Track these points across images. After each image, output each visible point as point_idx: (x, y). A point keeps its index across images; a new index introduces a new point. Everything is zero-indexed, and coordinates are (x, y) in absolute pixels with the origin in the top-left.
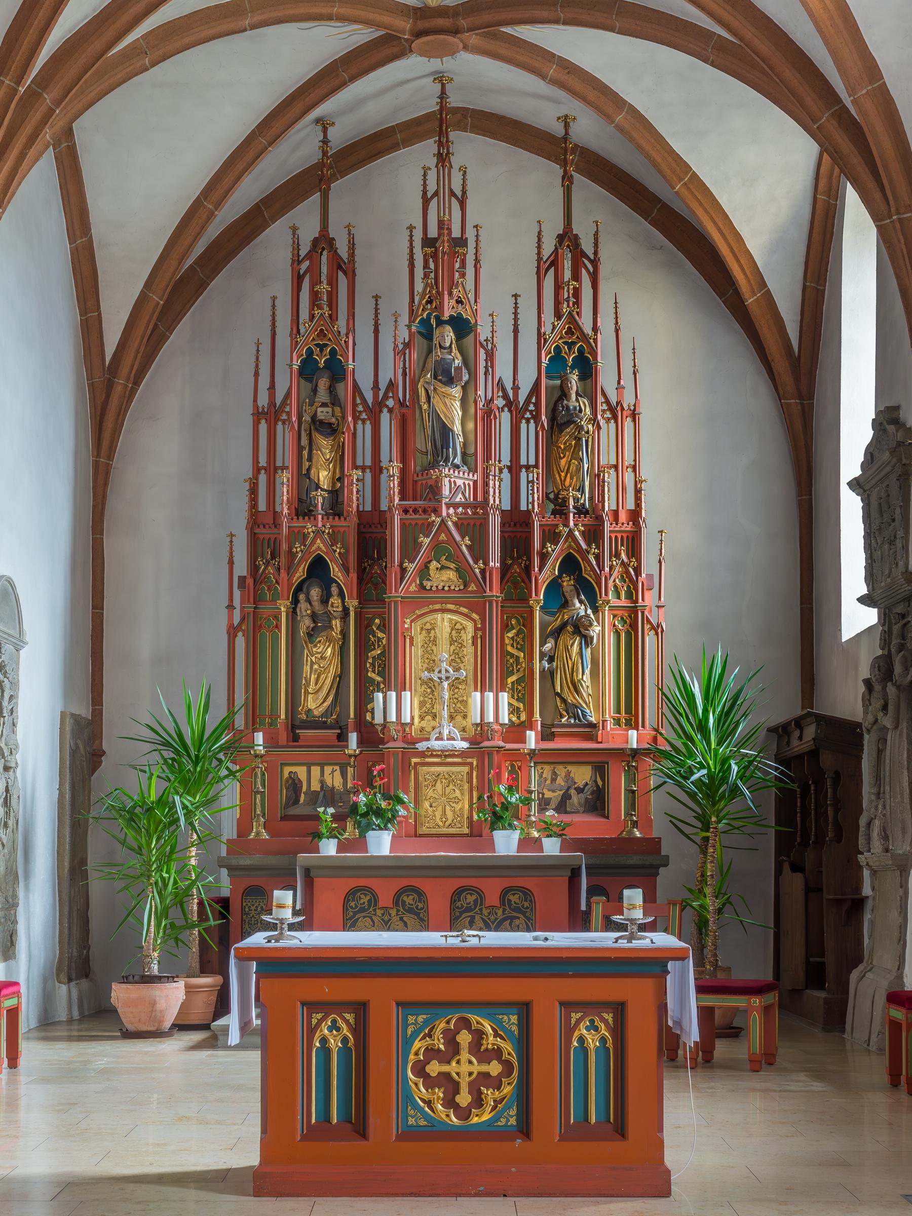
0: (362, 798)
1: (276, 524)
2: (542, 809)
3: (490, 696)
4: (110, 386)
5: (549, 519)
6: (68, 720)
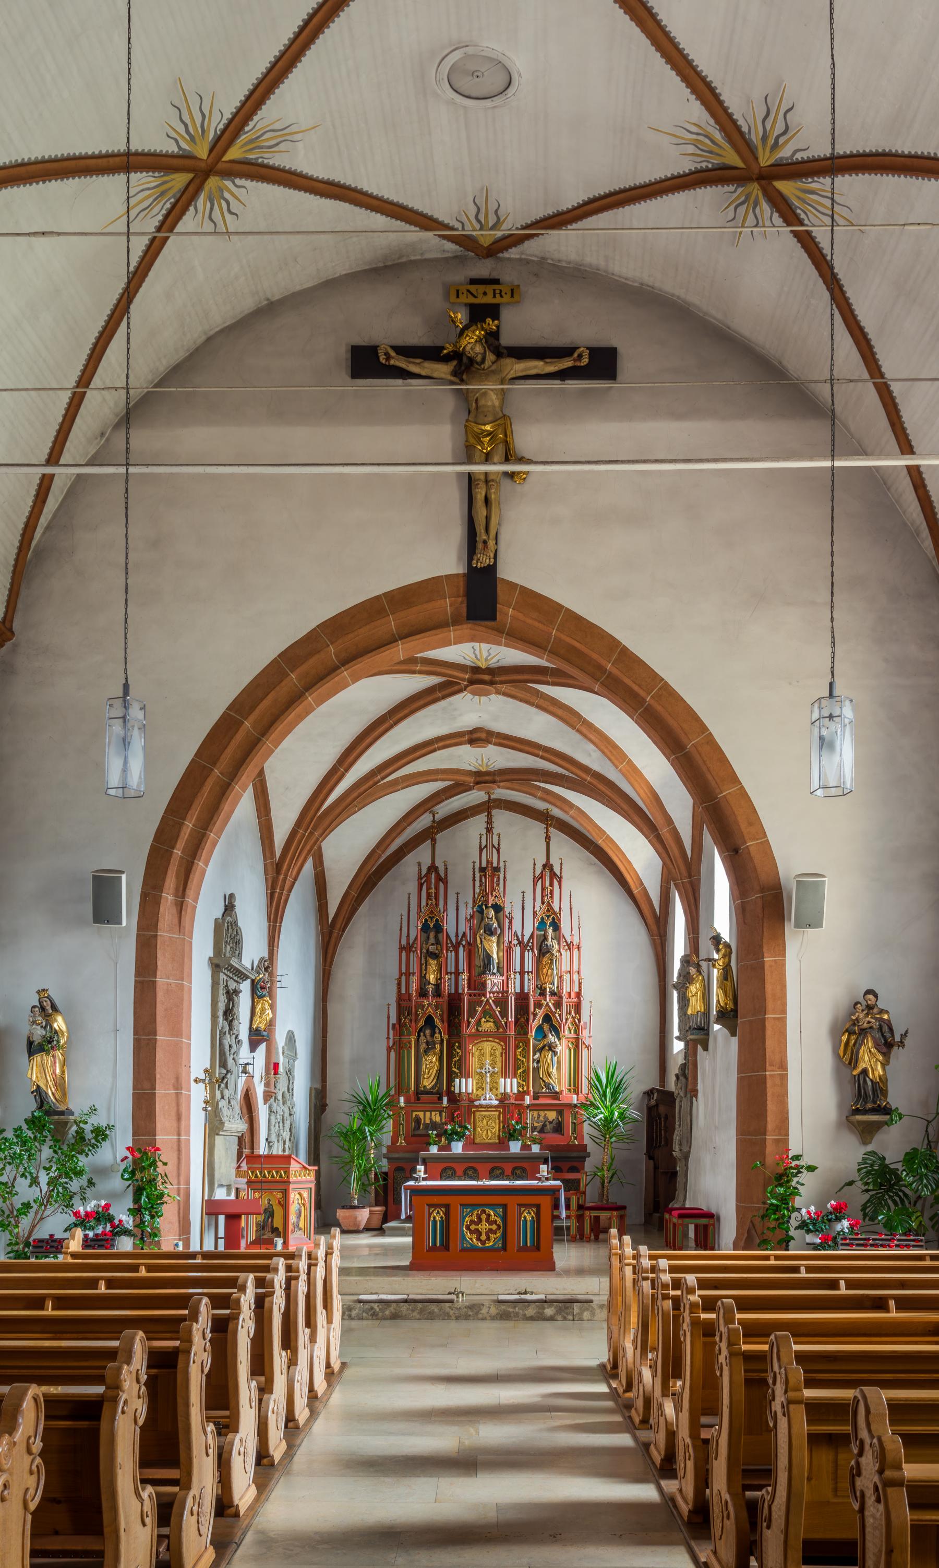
0: (449, 1127)
1: (410, 999)
2: (532, 1131)
3: (508, 1080)
4: (331, 933)
5: (538, 997)
6: (313, 1092)
